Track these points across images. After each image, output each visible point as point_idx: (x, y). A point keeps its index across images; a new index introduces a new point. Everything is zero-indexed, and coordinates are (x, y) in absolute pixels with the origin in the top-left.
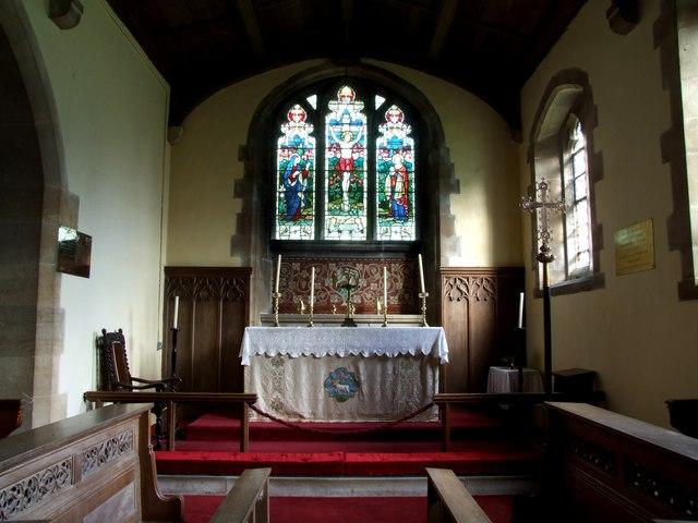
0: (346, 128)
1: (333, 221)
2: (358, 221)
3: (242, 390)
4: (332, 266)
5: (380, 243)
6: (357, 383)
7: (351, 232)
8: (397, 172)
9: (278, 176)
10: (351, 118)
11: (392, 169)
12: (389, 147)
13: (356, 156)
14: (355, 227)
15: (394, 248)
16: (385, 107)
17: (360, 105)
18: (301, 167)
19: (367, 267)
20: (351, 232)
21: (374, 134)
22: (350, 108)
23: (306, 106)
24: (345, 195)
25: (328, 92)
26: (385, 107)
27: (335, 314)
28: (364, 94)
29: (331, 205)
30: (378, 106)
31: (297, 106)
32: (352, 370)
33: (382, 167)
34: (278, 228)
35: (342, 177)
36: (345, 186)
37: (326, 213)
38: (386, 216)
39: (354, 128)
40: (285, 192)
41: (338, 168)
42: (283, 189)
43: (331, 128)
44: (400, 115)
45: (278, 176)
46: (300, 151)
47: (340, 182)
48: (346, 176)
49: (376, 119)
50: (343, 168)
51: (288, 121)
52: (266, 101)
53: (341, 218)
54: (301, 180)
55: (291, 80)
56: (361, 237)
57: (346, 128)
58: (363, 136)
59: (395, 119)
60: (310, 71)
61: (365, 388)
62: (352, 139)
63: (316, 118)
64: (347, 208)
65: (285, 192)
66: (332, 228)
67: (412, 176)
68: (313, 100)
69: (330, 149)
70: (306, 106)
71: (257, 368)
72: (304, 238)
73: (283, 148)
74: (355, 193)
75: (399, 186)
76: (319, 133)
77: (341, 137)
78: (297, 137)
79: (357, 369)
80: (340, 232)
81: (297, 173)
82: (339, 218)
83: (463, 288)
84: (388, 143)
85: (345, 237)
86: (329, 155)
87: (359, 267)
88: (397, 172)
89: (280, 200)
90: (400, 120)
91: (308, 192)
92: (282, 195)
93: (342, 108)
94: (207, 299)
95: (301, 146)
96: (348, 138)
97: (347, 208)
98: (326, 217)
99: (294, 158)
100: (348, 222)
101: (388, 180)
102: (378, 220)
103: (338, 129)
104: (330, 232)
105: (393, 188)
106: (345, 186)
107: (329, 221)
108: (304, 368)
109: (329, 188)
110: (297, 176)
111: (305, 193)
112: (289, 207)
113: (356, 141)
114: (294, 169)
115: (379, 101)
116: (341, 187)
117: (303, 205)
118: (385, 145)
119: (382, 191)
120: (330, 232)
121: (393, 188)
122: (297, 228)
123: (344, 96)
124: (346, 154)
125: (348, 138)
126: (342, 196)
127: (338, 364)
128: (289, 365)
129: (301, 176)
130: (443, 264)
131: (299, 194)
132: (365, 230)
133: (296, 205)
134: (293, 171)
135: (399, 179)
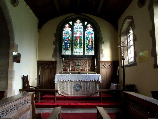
0: (78, 29)
1: (75, 50)
2: (81, 50)
3: (55, 89)
4: (75, 60)
5: (86, 55)
6: (81, 87)
7: (79, 53)
8: (90, 39)
9: (63, 40)
10: (79, 27)
11: (89, 38)
12: (88, 33)
13: (80, 36)
14: (80, 52)
15: (89, 57)
16: (87, 24)
17: (81, 24)
18: (68, 38)
19: (83, 61)
20: (79, 53)
21: (85, 30)
22: (79, 25)
23: (69, 24)
24: (78, 44)
25: (74, 21)
26: (87, 24)
27: (76, 71)
28: (82, 21)
29: (75, 47)
30: (85, 24)
31: (67, 24)
32: (80, 84)
33: (87, 38)
34: (63, 52)
35: (77, 40)
36: (78, 42)
37: (74, 48)
38: (87, 49)
39: (80, 29)
40: (64, 44)
41: (77, 38)
42: (64, 43)
43: (75, 29)
44: (91, 26)
45: (63, 40)
46: (68, 34)
47: (77, 41)
48: (78, 40)
49: (85, 27)
50: (78, 38)
51: (65, 28)
52: (60, 23)
53: (77, 50)
54: (68, 41)
55: (66, 18)
56: (82, 54)
57: (78, 29)
58: (82, 31)
59: (89, 27)
60: (70, 16)
61: (83, 88)
62: (80, 32)
63: (72, 27)
64: (78, 47)
65: (64, 44)
66: (75, 52)
67: (93, 40)
68: (71, 23)
69: (75, 34)
70: (69, 24)
71: (58, 84)
72: (69, 54)
73: (64, 34)
74: (80, 44)
75: (90, 42)
76: (72, 30)
77: (77, 31)
78: (67, 31)
79: (81, 84)
80: (77, 53)
81: (67, 39)
82: (77, 50)
83: (105, 66)
84: (88, 32)
85: (78, 54)
86: (74, 35)
87: (81, 61)
88: (90, 39)
89: (63, 45)
90: (90, 27)
91: (70, 44)
92: (64, 44)
93: (77, 25)
94: (47, 68)
95: (68, 33)
96: (79, 31)
97: (78, 47)
98: (74, 49)
99: (66, 36)
100: (79, 50)
101: (88, 41)
102: (86, 50)
103: (76, 29)
104: (75, 53)
105: (89, 43)
106: (78, 42)
107: (75, 50)
108: (69, 84)
109: (75, 43)
110: (67, 40)
111: (69, 44)
112: (65, 47)
113: (81, 32)
114: (67, 39)
115: (86, 23)
116: (77, 43)
117: (69, 47)
118: (87, 33)
119: (87, 43)
120: (75, 53)
121: (89, 43)
122: (67, 52)
123: (78, 22)
124: (78, 35)
125: (79, 31)
126: (77, 45)
127: (76, 83)
128: (65, 83)
129: (68, 40)
130: (100, 60)
131: (68, 44)
132: (83, 52)
133: (67, 47)
134: (66, 39)
135: (90, 41)
